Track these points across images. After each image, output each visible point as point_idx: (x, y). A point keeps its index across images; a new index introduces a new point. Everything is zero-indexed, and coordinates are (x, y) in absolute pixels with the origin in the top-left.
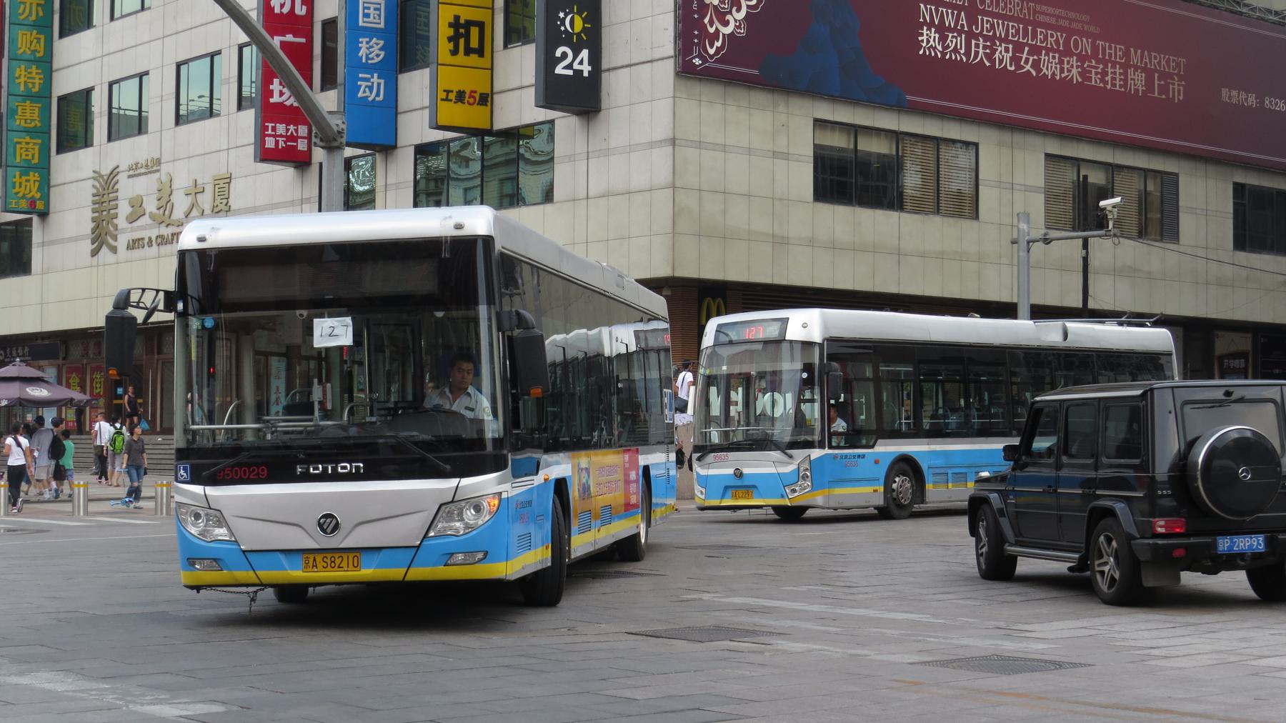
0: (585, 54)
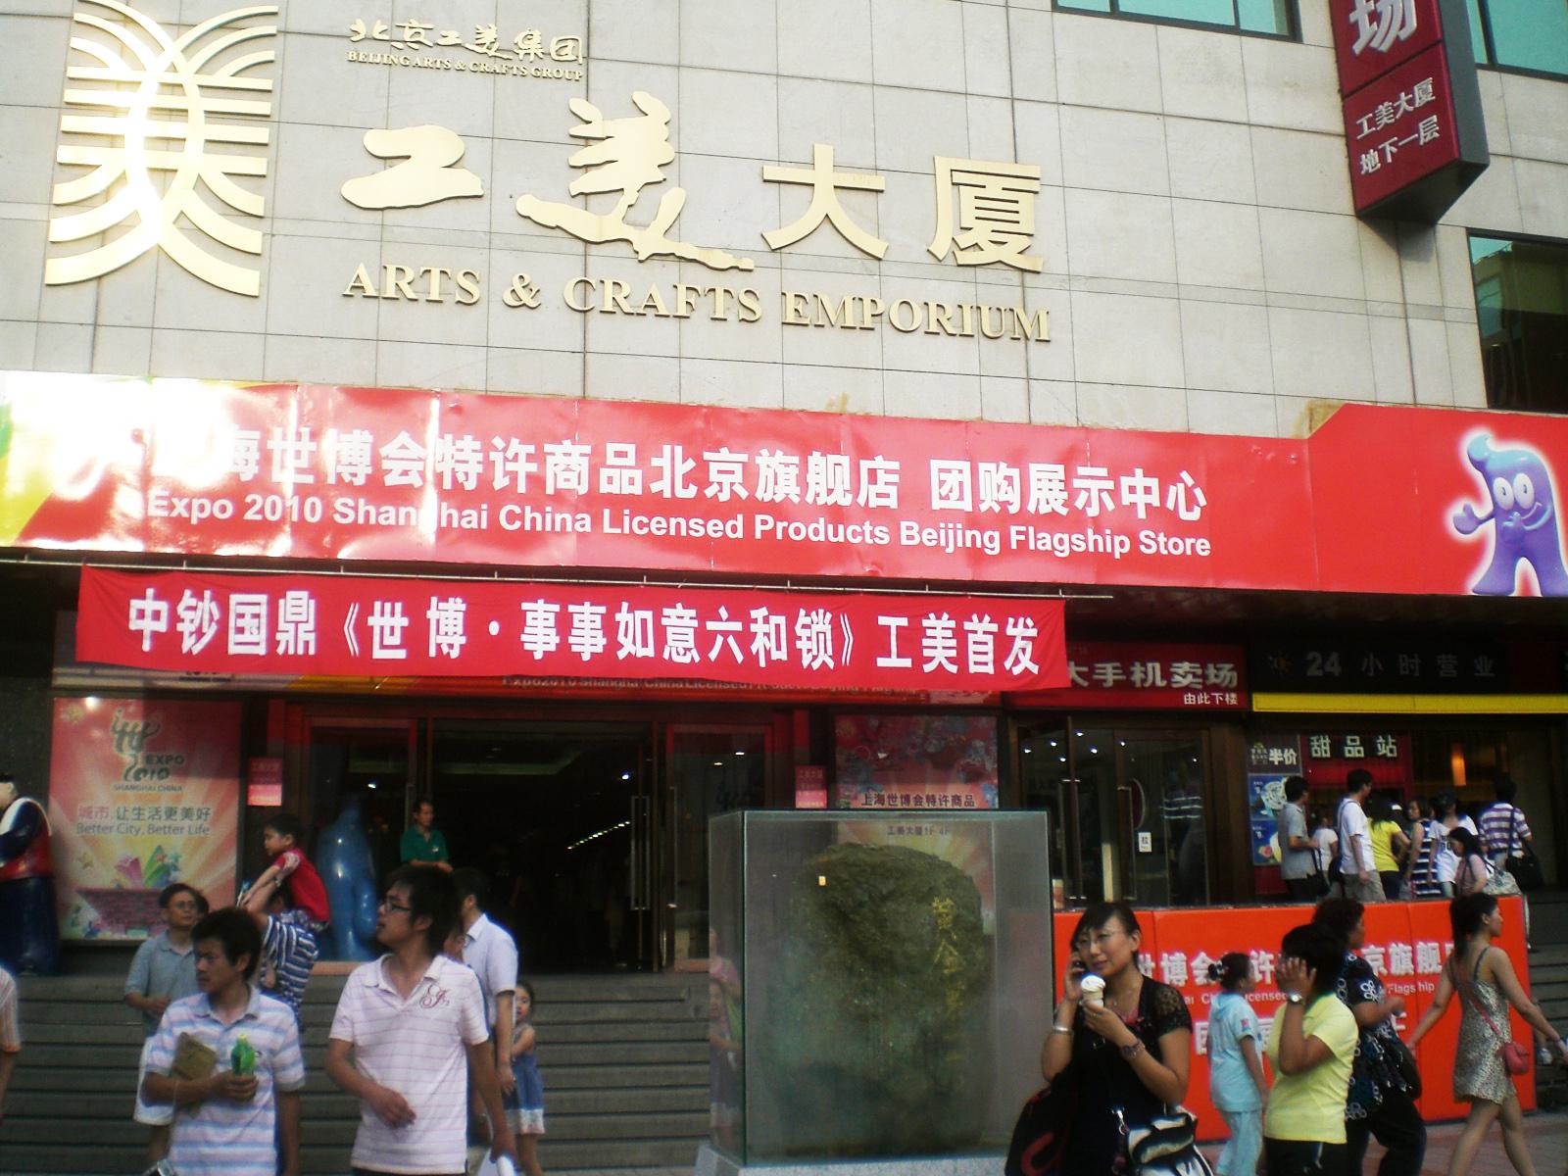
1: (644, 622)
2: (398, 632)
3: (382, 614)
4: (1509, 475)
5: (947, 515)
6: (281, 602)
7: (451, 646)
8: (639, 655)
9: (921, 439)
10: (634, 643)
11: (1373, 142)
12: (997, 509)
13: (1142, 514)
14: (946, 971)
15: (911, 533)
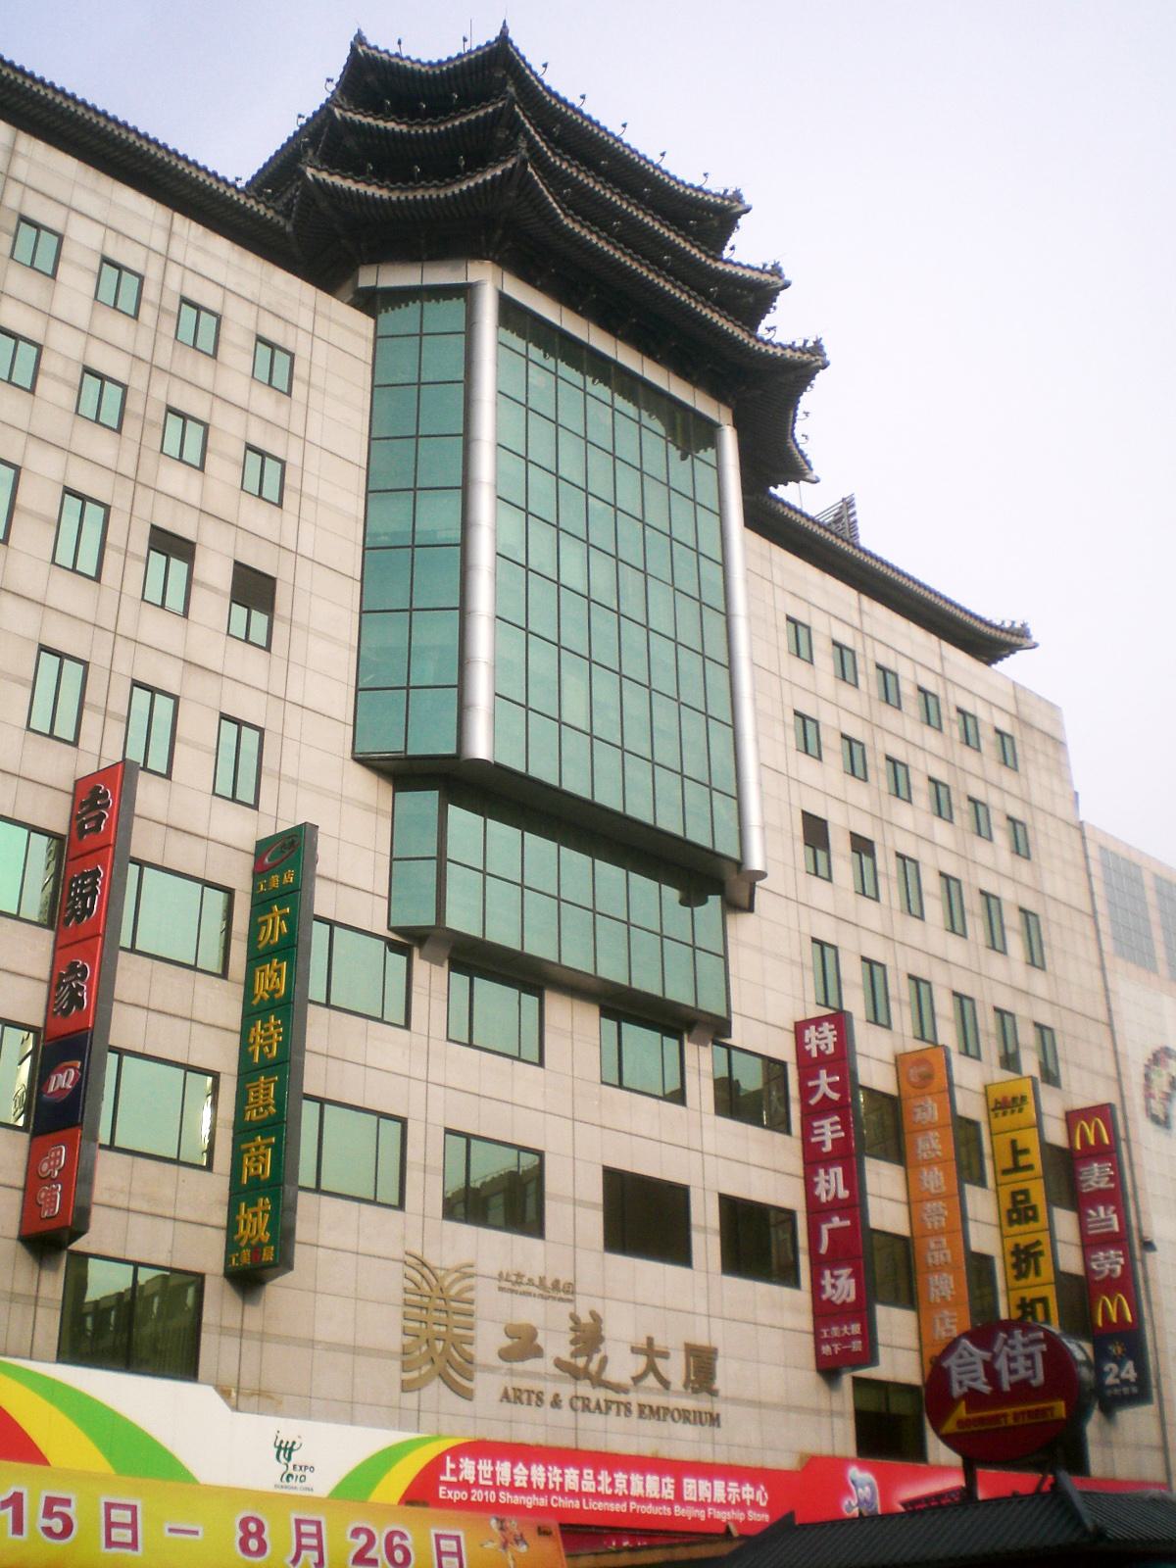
0: (1130, 1365)
4: (863, 1487)
5: (690, 1503)
9: (678, 1469)
11: (829, 1341)
12: (267, 996)
13: (748, 1503)
15: (679, 1511)
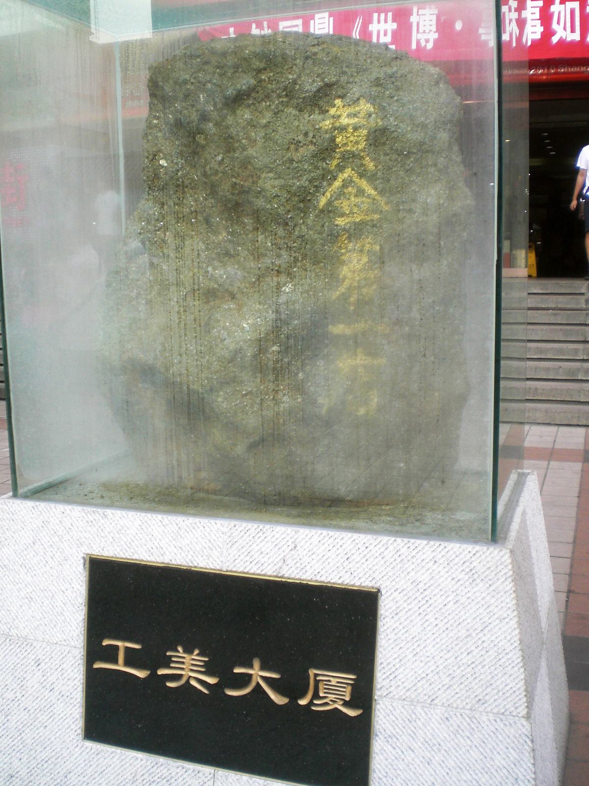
1: (572, 12)
2: (389, 34)
3: (379, 22)
6: (312, 22)
7: (427, 41)
8: (569, 39)
10: (565, 29)
14: (340, 222)
